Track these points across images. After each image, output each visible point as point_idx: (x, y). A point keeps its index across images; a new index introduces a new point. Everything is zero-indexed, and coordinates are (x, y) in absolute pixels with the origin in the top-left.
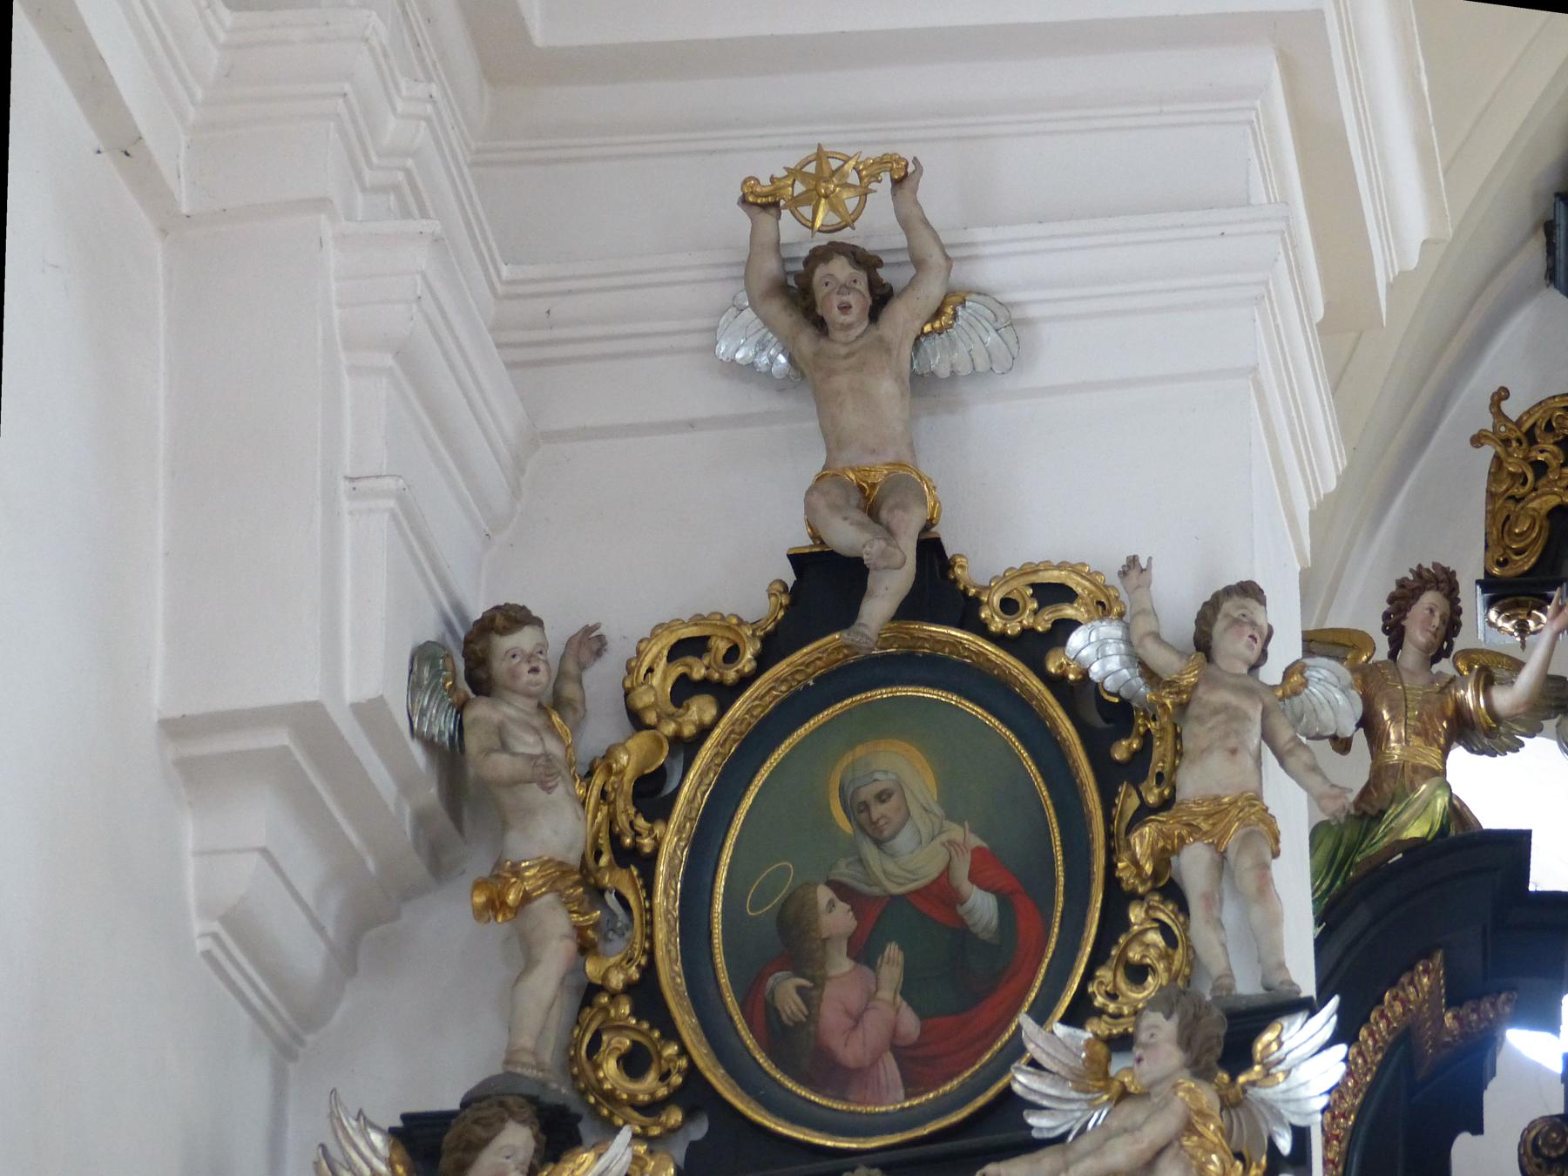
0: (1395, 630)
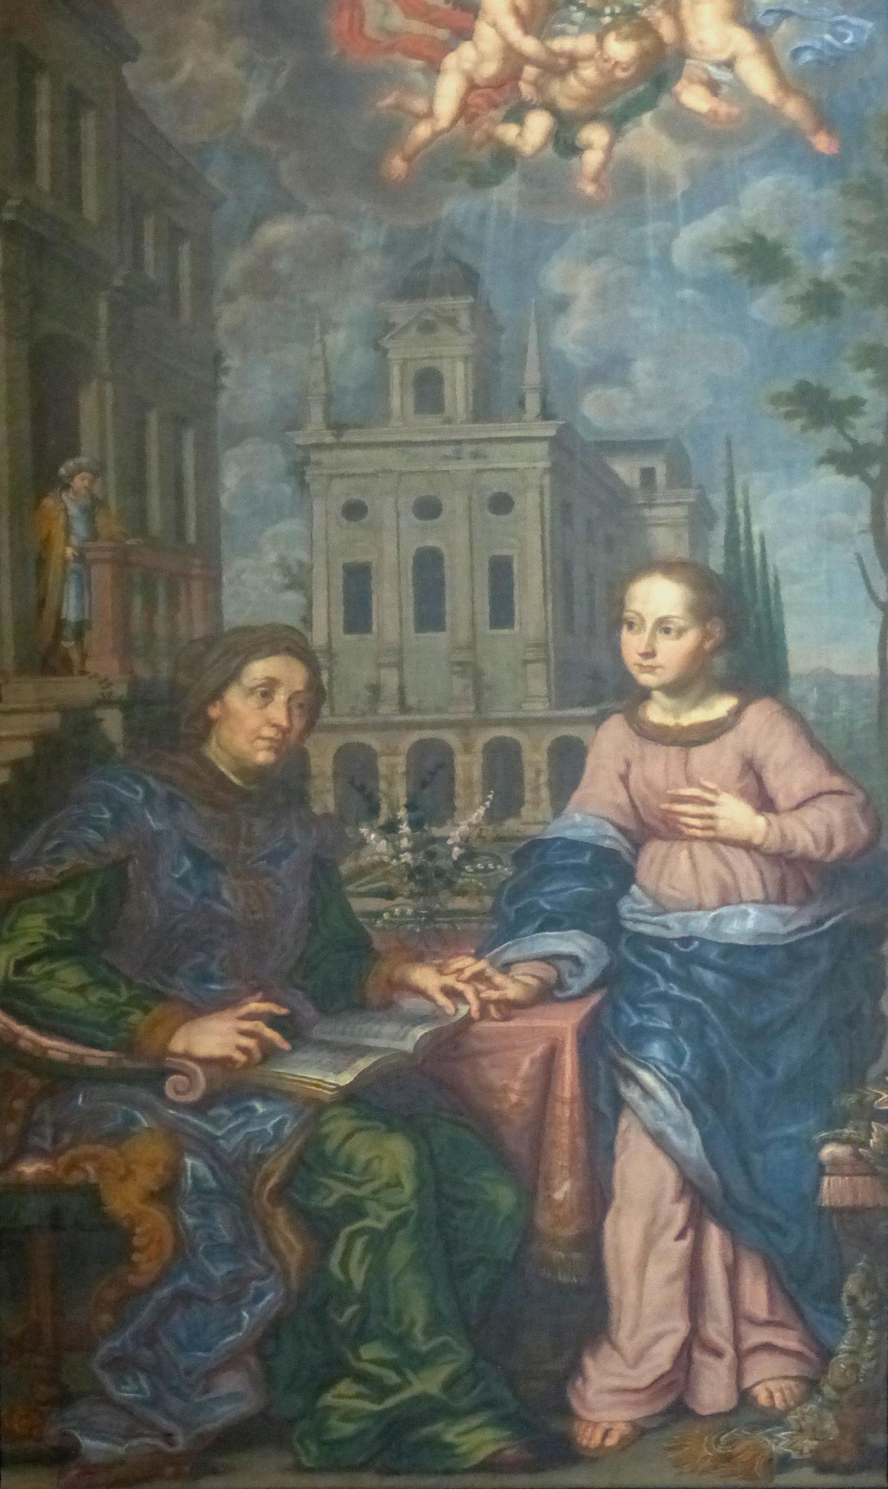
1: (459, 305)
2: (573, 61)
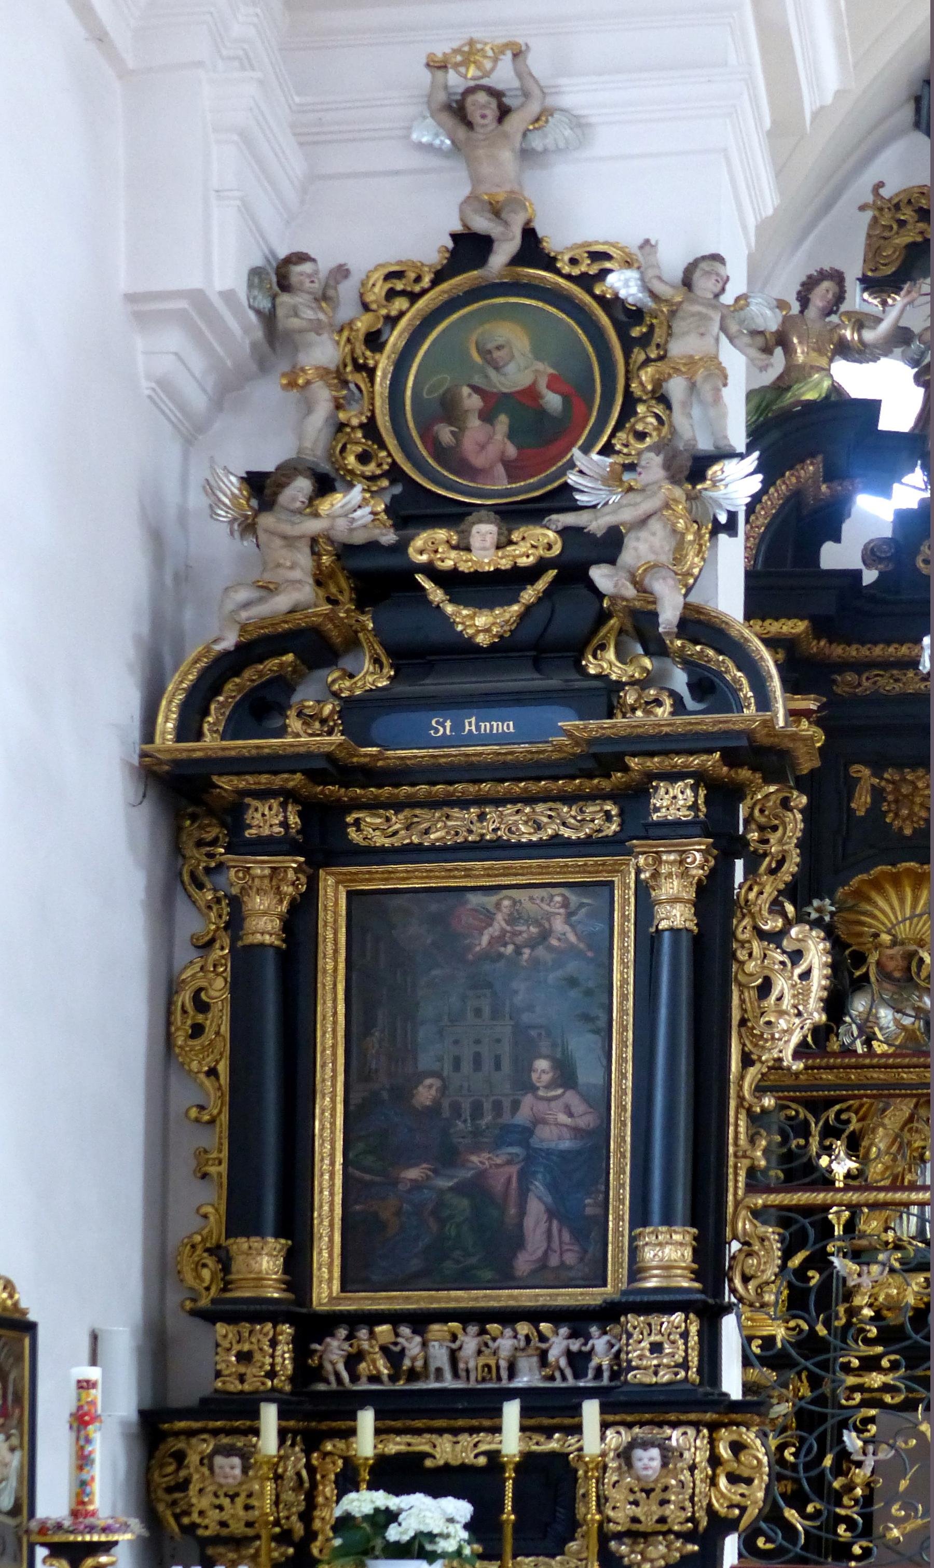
0: (804, 299)
1: (488, 992)
2: (521, 933)
